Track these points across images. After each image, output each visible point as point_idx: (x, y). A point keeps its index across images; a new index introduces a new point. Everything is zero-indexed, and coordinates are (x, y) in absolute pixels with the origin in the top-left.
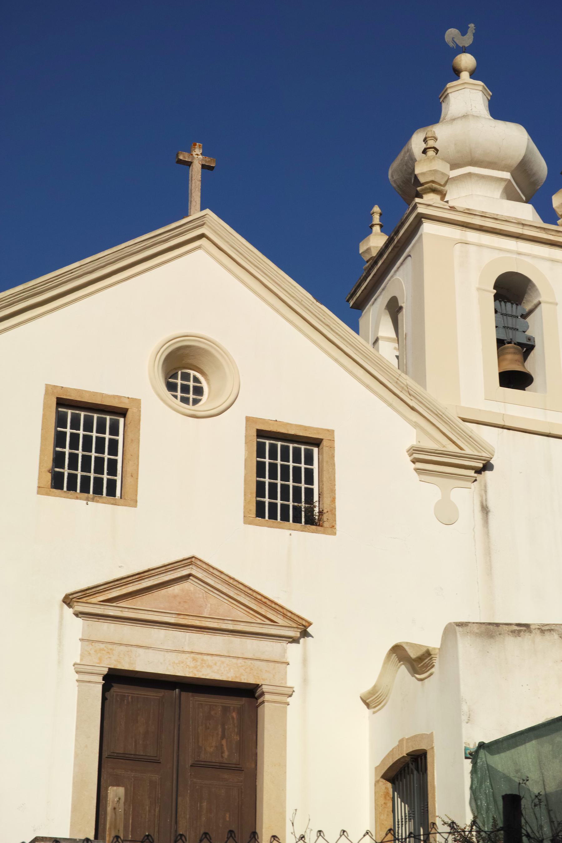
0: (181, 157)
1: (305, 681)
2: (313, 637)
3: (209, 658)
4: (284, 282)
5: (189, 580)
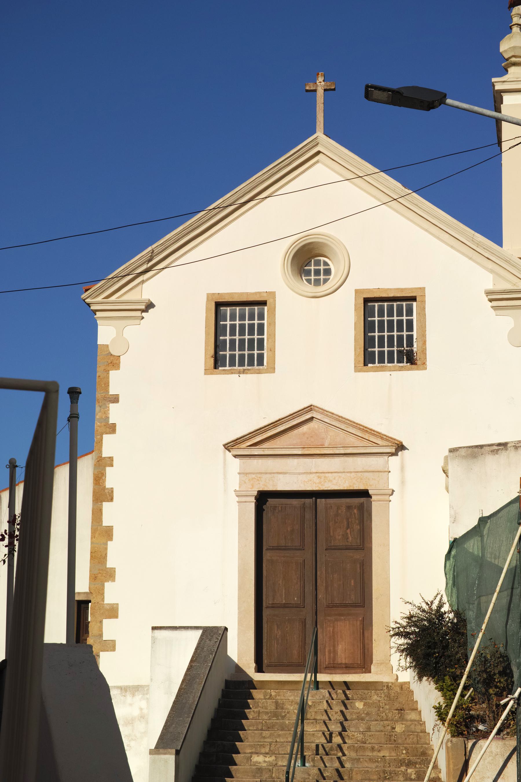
0: (307, 88)
1: (403, 482)
2: (408, 450)
3: (330, 475)
4: (380, 178)
5: (314, 421)
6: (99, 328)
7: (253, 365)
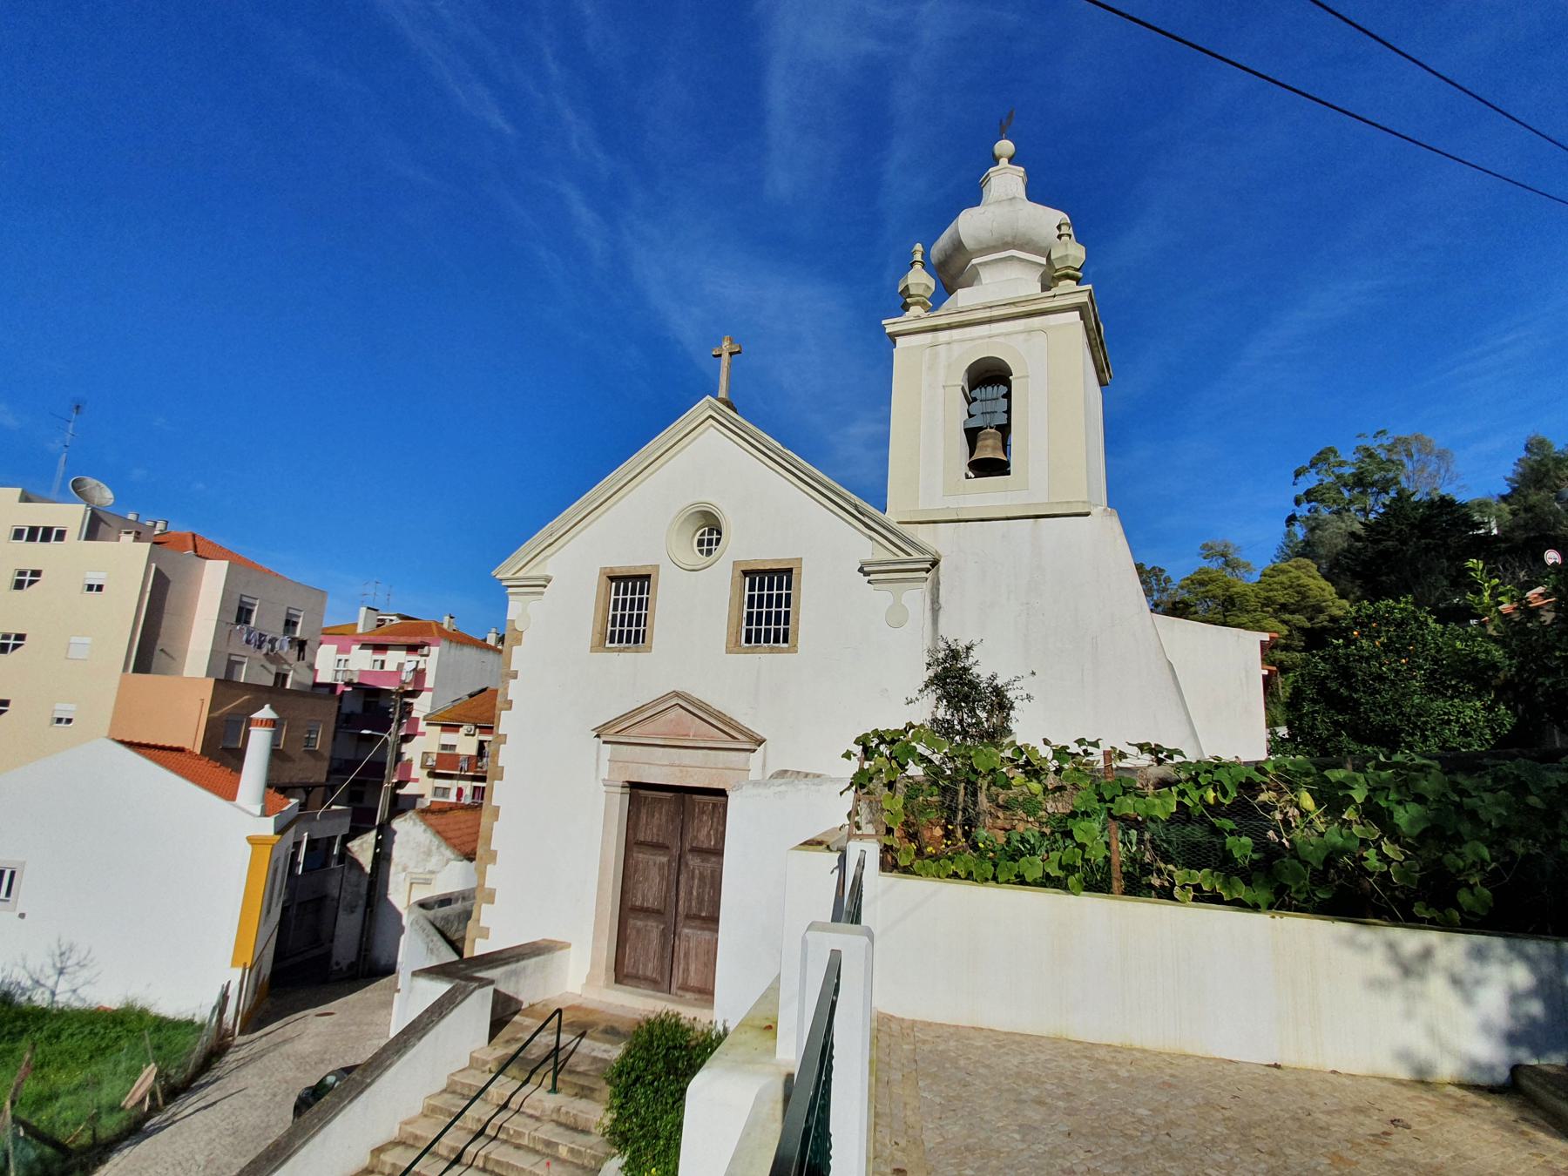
6: (510, 603)
7: (779, 642)
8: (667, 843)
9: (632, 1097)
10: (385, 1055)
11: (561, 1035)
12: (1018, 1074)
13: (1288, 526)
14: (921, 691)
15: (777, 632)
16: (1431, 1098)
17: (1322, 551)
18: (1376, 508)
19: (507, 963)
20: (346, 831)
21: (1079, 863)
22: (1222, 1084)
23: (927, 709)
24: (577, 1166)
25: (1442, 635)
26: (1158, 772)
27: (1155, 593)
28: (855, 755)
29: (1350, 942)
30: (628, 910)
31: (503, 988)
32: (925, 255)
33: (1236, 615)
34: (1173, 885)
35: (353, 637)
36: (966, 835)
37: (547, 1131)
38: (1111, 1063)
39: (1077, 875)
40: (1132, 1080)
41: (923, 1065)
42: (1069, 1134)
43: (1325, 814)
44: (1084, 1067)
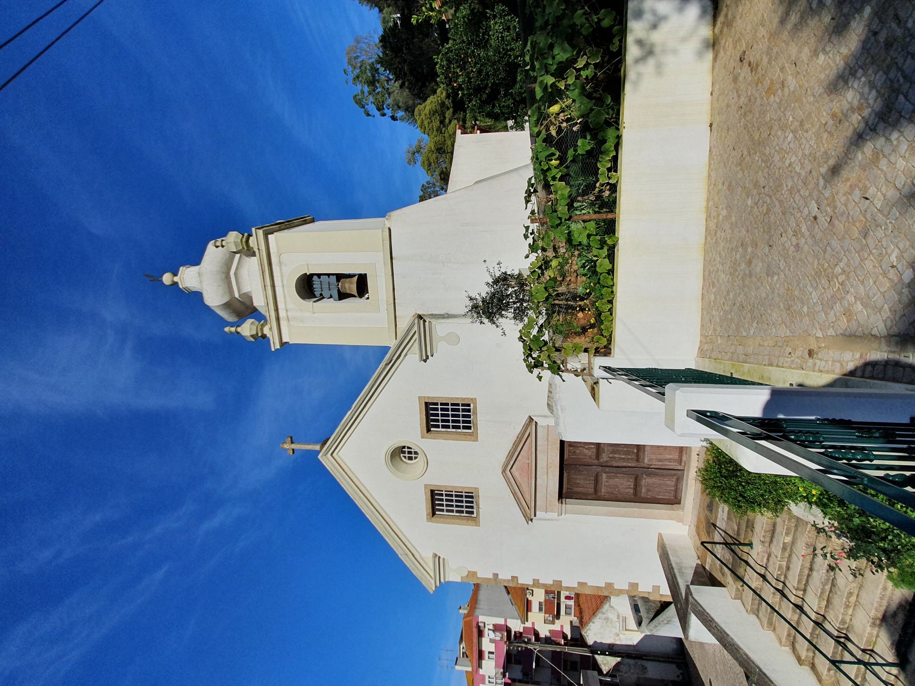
7: (471, 427)
8: (595, 474)
9: (753, 499)
10: (740, 659)
11: (715, 541)
12: (731, 274)
13: (397, 120)
14: (497, 326)
15: (463, 410)
16: (724, 41)
17: (411, 102)
18: (386, 74)
19: (675, 575)
20: (595, 673)
21: (598, 238)
22: (726, 156)
23: (510, 326)
24: (796, 530)
25: (454, 40)
26: (541, 193)
27: (436, 189)
28: (540, 373)
29: (635, 84)
30: (636, 497)
31: (690, 578)
32: (232, 324)
33: (447, 147)
34: (608, 183)
35: (474, 674)
36: (582, 299)
37: (776, 550)
38: (718, 219)
39: (606, 239)
40: (729, 207)
41: (731, 332)
42: (770, 246)
43: (561, 99)
44: (723, 235)
